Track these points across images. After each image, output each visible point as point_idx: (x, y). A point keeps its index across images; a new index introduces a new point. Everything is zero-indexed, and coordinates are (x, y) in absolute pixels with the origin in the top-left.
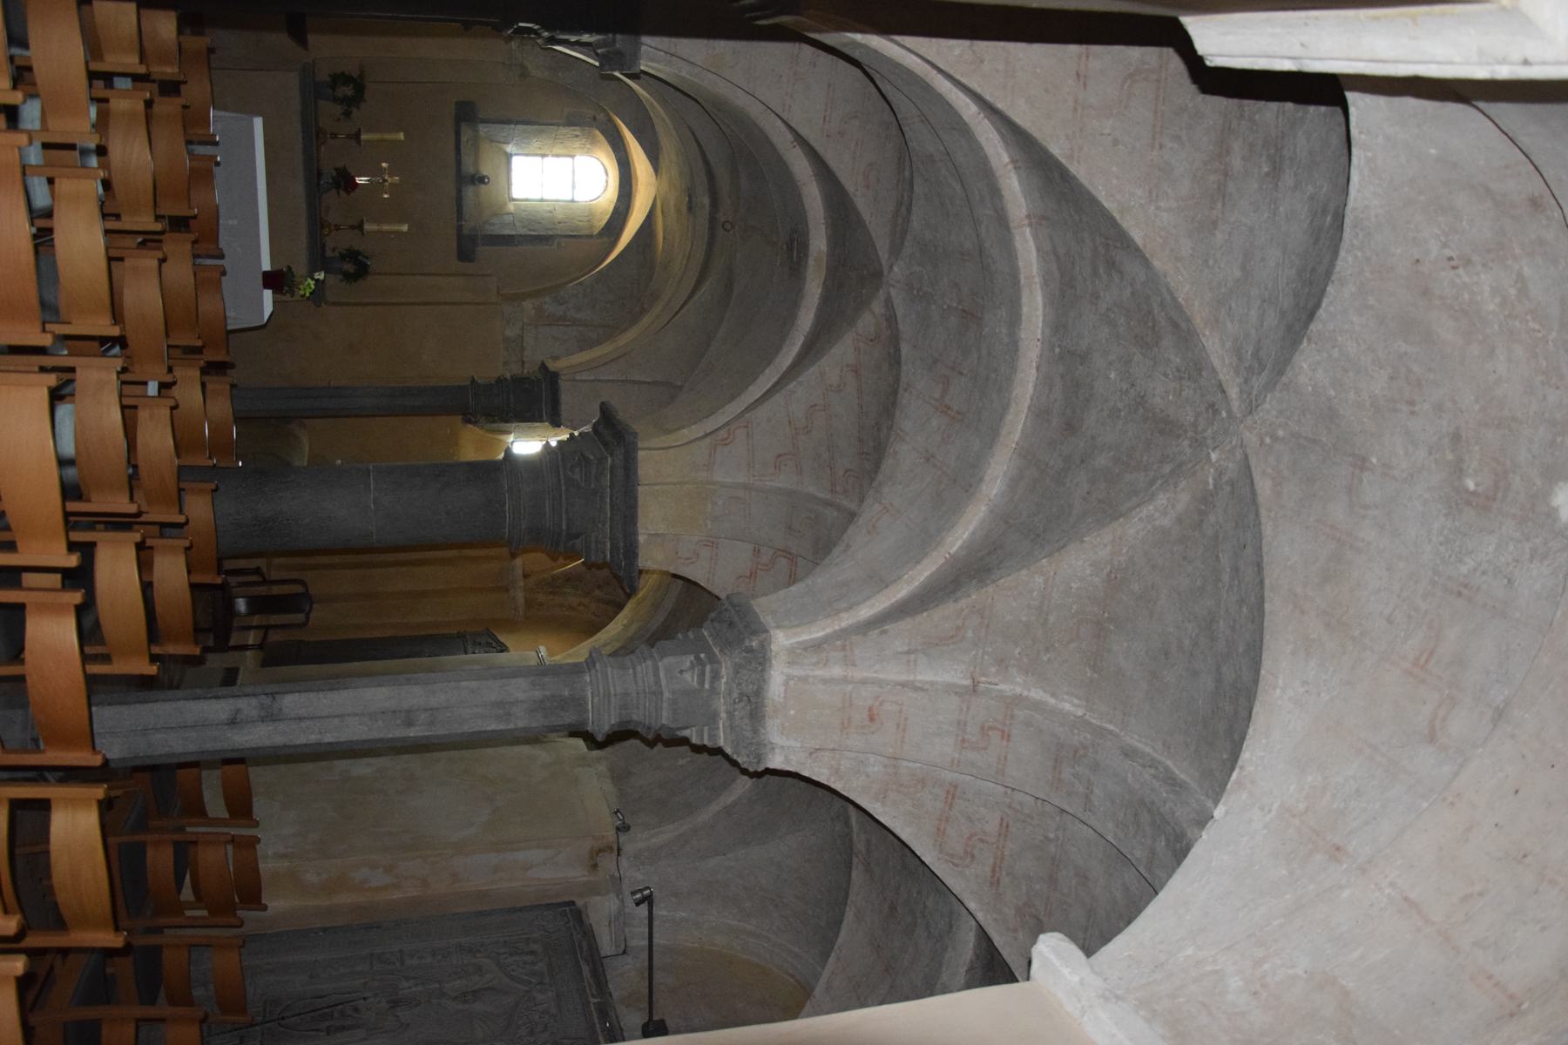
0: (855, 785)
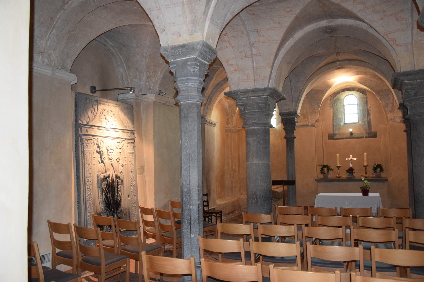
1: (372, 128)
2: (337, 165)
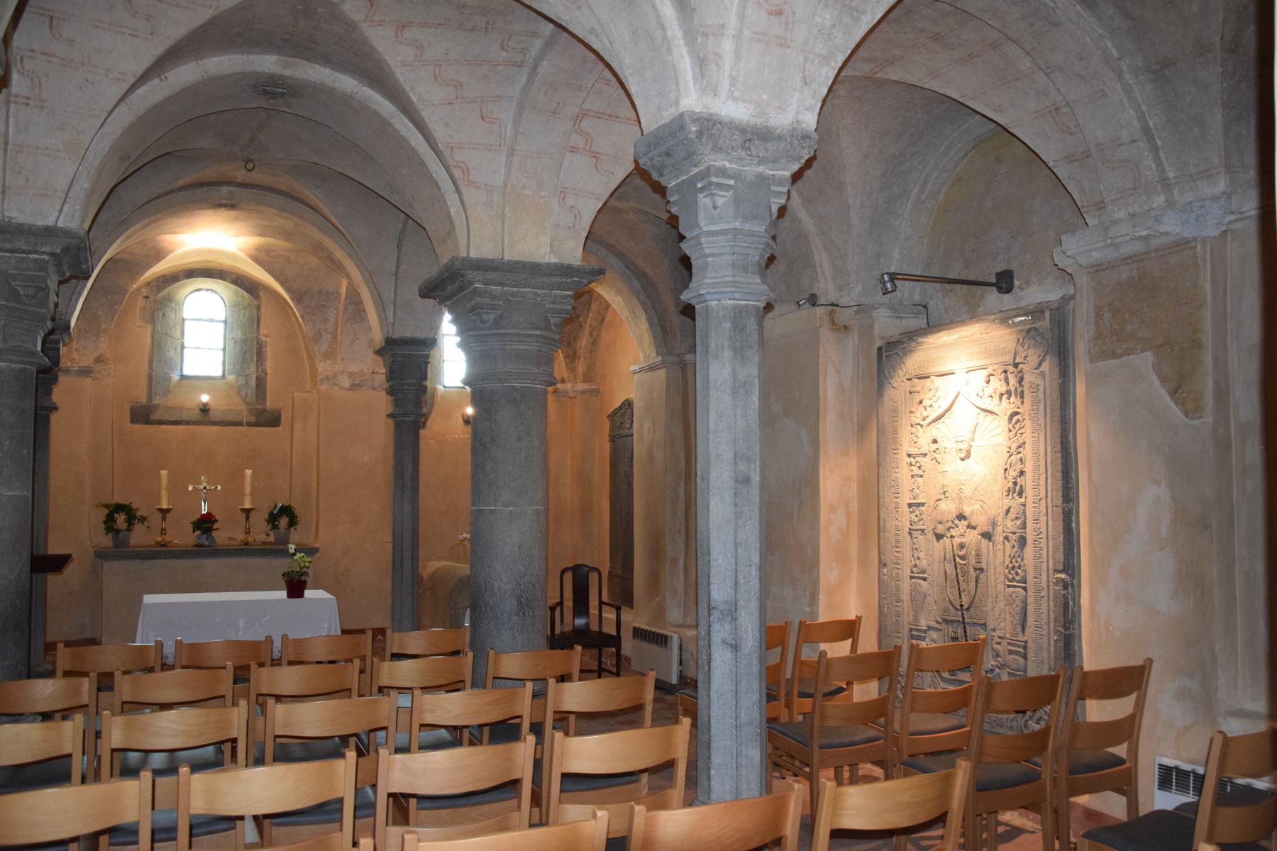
0: (842, 41)
1: (268, 397)
2: (159, 502)
